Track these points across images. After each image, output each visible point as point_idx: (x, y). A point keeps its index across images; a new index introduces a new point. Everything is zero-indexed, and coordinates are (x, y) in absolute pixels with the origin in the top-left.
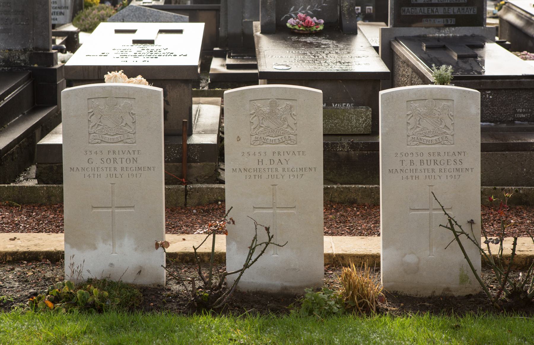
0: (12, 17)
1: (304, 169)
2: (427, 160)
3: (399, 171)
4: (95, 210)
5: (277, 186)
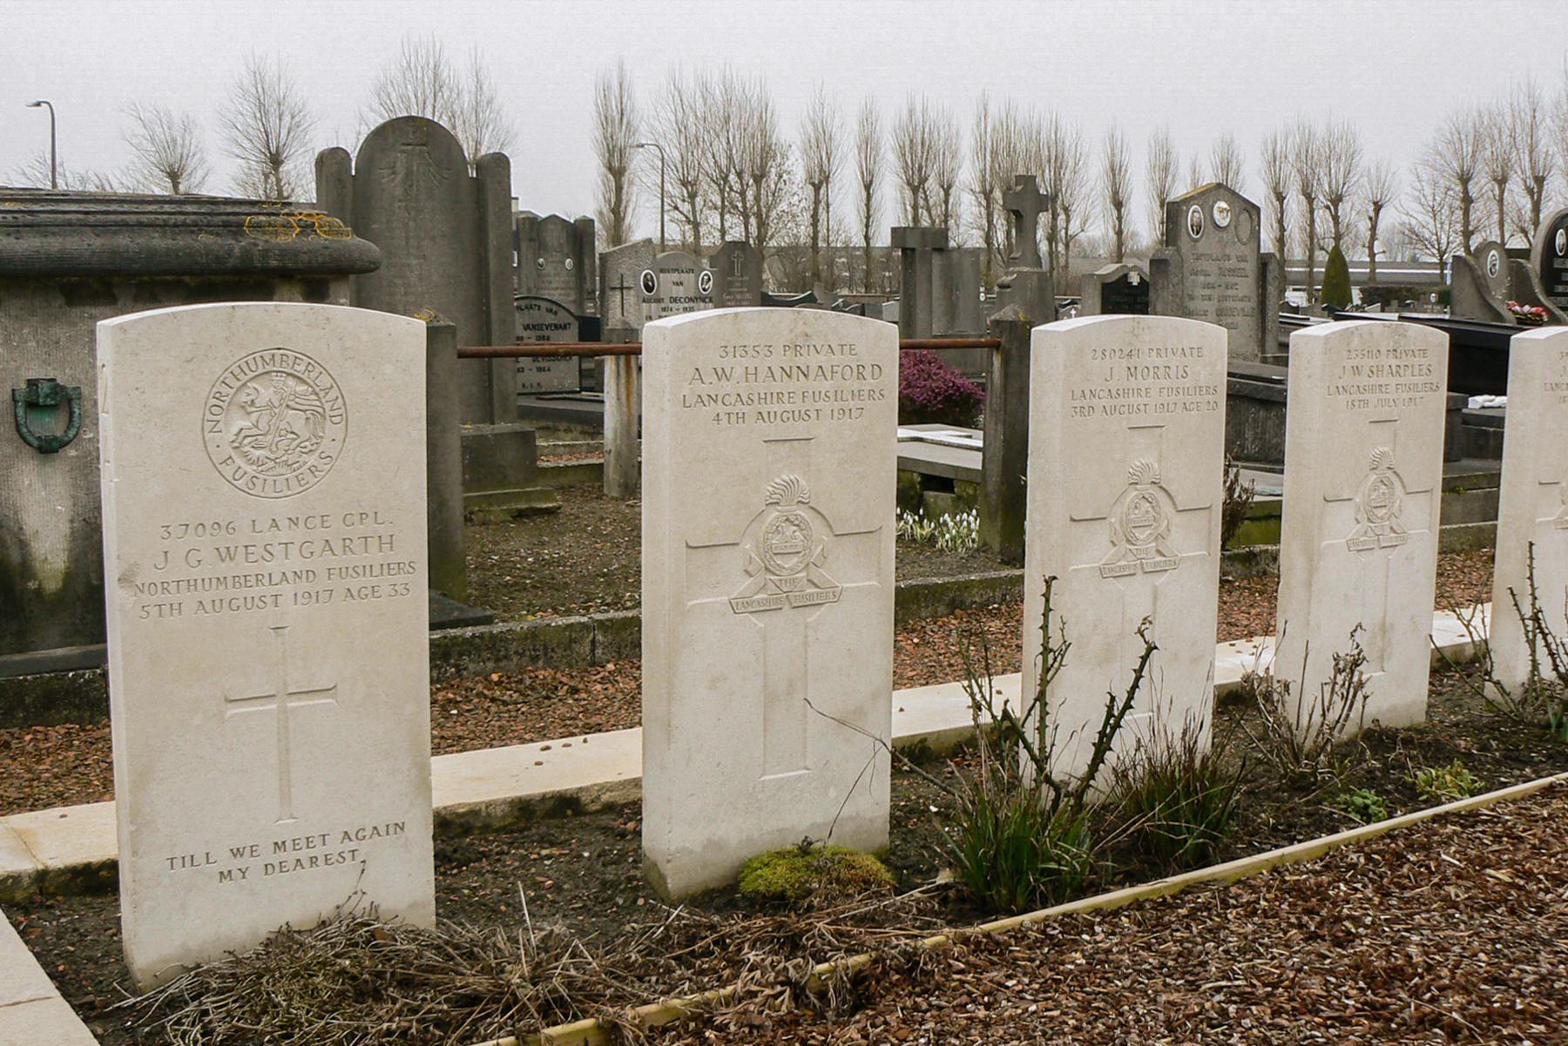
1: (230, 581)
2: (183, 858)
3: (290, 576)
5: (286, 631)
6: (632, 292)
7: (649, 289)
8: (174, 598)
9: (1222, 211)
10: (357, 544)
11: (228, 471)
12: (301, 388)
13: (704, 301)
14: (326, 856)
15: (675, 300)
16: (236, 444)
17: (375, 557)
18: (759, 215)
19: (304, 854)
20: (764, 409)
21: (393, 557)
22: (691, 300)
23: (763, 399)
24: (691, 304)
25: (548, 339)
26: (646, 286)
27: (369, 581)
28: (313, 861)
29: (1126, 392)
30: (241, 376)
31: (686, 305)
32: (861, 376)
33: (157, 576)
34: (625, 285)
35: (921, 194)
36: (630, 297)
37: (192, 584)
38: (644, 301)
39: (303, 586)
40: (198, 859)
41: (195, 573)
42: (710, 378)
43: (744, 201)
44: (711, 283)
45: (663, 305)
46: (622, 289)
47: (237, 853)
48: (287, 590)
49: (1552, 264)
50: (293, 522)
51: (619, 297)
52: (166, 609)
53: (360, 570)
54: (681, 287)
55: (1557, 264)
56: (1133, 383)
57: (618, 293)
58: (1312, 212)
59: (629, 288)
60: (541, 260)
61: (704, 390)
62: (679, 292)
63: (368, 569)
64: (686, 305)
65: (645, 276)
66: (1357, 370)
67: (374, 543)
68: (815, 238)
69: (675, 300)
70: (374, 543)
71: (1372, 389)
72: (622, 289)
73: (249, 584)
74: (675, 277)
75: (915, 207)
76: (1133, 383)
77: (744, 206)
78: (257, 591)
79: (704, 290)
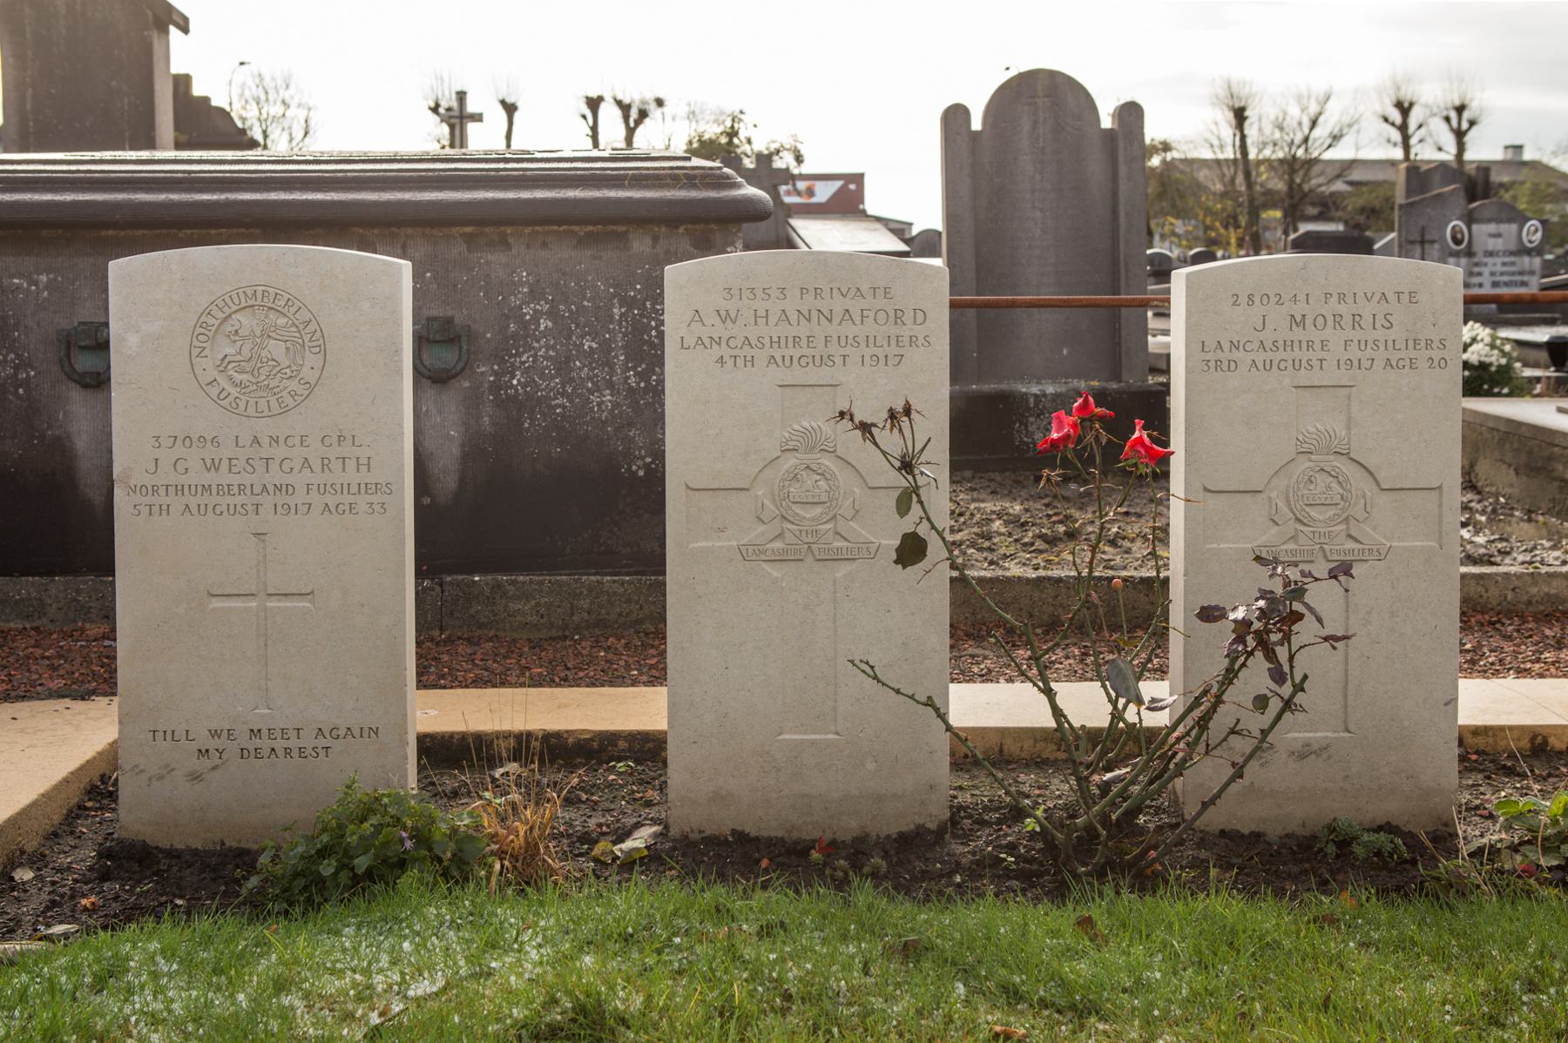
4: (217, 603)
6: (1436, 246)
7: (1457, 242)
10: (336, 466)
11: (214, 392)
15: (1491, 254)
16: (221, 368)
17: (352, 476)
19: (279, 744)
21: (370, 479)
22: (1512, 253)
23: (775, 343)
24: (1512, 259)
28: (287, 751)
30: (226, 309)
31: (1506, 260)
33: (148, 480)
34: (1427, 237)
37: (180, 490)
39: (281, 499)
40: (181, 734)
44: (1539, 235)
45: (1476, 260)
46: (1422, 242)
47: (215, 734)
48: (267, 501)
52: (156, 509)
53: (338, 488)
54: (1500, 241)
56: (1298, 334)
59: (1432, 242)
61: (704, 333)
62: (1498, 244)
63: (345, 486)
64: (1506, 260)
65: (1453, 227)
67: (351, 465)
69: (1491, 254)
70: (351, 465)
72: (1422, 242)
73: (232, 492)
74: (1492, 228)
78: (239, 500)
79: (1530, 242)
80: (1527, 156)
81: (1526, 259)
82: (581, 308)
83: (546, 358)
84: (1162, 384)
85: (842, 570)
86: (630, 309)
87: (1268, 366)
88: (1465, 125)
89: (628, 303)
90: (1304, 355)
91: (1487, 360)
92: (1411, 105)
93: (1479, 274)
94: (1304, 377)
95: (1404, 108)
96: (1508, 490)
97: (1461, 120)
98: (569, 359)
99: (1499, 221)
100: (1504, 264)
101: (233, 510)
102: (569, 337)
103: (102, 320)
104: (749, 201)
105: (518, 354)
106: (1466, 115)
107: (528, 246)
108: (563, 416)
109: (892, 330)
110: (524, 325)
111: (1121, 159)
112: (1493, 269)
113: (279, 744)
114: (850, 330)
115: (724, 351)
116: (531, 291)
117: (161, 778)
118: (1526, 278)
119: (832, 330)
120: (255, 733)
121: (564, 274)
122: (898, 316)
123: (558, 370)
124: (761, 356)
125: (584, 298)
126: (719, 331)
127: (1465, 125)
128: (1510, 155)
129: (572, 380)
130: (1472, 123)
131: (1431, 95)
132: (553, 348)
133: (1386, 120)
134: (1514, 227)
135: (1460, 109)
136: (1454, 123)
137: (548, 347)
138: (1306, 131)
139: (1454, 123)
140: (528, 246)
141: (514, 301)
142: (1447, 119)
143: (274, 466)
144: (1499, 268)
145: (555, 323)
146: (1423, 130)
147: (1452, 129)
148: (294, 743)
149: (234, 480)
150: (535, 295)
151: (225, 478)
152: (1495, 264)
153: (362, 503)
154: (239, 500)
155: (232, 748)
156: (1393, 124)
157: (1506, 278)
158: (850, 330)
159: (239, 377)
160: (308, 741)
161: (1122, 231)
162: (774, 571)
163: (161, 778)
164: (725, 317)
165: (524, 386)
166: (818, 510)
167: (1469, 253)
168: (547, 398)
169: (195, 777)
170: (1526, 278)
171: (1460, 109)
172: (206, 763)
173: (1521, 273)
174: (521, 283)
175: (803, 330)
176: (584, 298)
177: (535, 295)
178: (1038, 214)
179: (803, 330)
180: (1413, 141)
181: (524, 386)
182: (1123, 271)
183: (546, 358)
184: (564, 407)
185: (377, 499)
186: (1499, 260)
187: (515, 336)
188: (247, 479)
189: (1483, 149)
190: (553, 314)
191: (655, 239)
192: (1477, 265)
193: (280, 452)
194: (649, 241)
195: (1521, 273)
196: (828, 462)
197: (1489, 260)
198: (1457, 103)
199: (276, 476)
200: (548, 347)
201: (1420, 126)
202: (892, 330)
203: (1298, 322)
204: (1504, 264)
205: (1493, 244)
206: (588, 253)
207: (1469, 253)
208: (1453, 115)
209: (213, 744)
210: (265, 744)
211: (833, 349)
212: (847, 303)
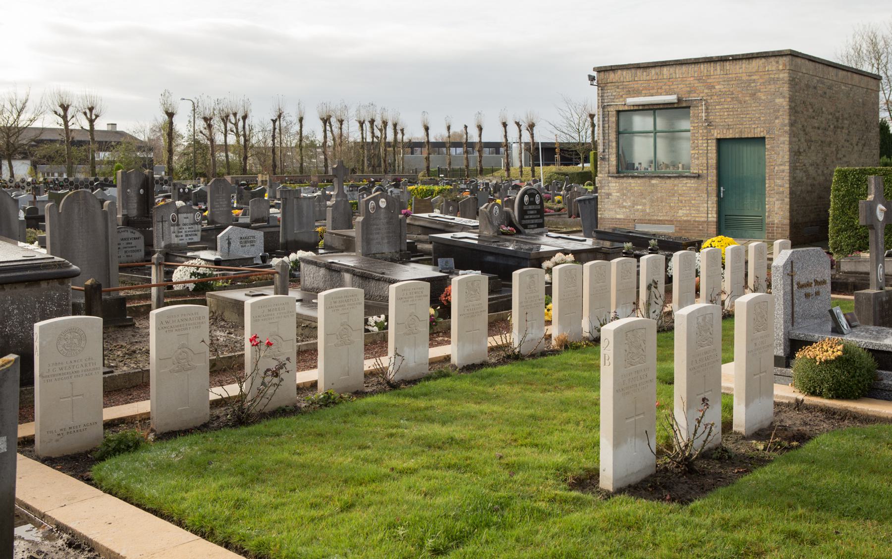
0: (391, 235)
4: (62, 400)
8: (50, 378)
9: (382, 202)
10: (88, 365)
11: (62, 352)
12: (77, 334)
13: (197, 224)
14: (288, 303)
15: (185, 225)
17: (92, 367)
18: (245, 135)
19: (75, 430)
20: (177, 329)
21: (96, 367)
22: (192, 224)
23: (177, 326)
25: (131, 243)
26: (173, 220)
27: (91, 372)
28: (77, 431)
29: (268, 315)
32: (200, 319)
33: (47, 374)
34: (164, 219)
35: (328, 124)
36: (166, 225)
37: (54, 375)
38: (172, 226)
40: (54, 431)
41: (55, 373)
42: (164, 323)
43: (237, 129)
46: (162, 222)
47: (61, 430)
48: (73, 375)
49: (523, 208)
50: (75, 361)
51: (161, 225)
54: (188, 220)
55: (525, 208)
56: (270, 313)
57: (161, 223)
58: (520, 131)
59: (166, 221)
60: (128, 190)
61: (163, 326)
62: (187, 221)
66: (335, 302)
67: (91, 365)
68: (274, 144)
69: (185, 225)
70: (91, 365)
71: (340, 306)
72: (162, 222)
74: (185, 215)
75: (325, 131)
76: (270, 313)
77: (237, 131)
78: (67, 376)
80: (118, 129)
81: (196, 226)
82: (27, 306)
83: (16, 322)
84: (313, 343)
85: (189, 372)
86: (41, 304)
87: (265, 320)
88: (94, 117)
89: (41, 303)
90: (270, 317)
91: (205, 272)
92: (68, 106)
93: (181, 232)
94: (271, 321)
95: (65, 108)
96: (236, 321)
97: (91, 113)
98: (23, 321)
99: (187, 213)
100: (189, 228)
101: (65, 378)
102: (23, 315)
103: (509, 294)
104: (74, 271)
105: (8, 322)
106: (94, 112)
107: (11, 289)
108: (21, 338)
109: (198, 321)
110: (10, 313)
111: (109, 221)
112: (186, 230)
113: (75, 430)
114: (191, 322)
115: (167, 329)
116: (12, 302)
117: (49, 442)
118: (196, 233)
119: (187, 322)
120: (70, 428)
121: (22, 296)
122: (199, 318)
123: (20, 325)
124: (174, 329)
125: (27, 302)
126: (166, 325)
127: (94, 117)
128: (110, 128)
129: (24, 327)
130: (97, 116)
131: (77, 104)
132: (18, 318)
133: (56, 113)
134: (192, 214)
135: (91, 109)
136: (89, 116)
137: (17, 318)
138: (15, 117)
139: (89, 116)
140: (11, 289)
141: (6, 306)
142: (85, 114)
143: (75, 367)
144: (188, 230)
145: (19, 311)
146: (74, 119)
147: (87, 118)
148: (79, 429)
149: (66, 371)
150: (13, 303)
151: (64, 371)
152: (186, 228)
153: (94, 372)
154: (67, 376)
155: (65, 433)
156: (60, 115)
157: (190, 233)
158: (191, 322)
159: (67, 348)
160: (82, 428)
161: (110, 245)
162: (176, 374)
163: (49, 442)
164: (167, 322)
165: (10, 331)
166: (185, 360)
167: (178, 225)
168: (17, 334)
169: (57, 441)
170: (196, 233)
171: (91, 109)
172: (59, 437)
173: (195, 231)
174: (8, 300)
175: (182, 323)
176: (27, 302)
177: (13, 303)
178: (81, 240)
179: (182, 323)
180: (70, 124)
181: (10, 331)
182: (110, 259)
183: (16, 322)
184: (22, 336)
185: (97, 371)
186: (187, 227)
187: (7, 316)
188: (69, 371)
189: (101, 125)
190: (18, 308)
191: (48, 283)
192: (180, 229)
193: (76, 364)
194: (46, 284)
195: (195, 231)
196: (187, 350)
197: (184, 227)
198: (90, 106)
199: (76, 369)
200: (17, 318)
201: (73, 117)
202: (198, 321)
203: (269, 310)
204: (189, 228)
205: (186, 221)
206: (28, 289)
207: (178, 225)
208: (88, 111)
209: (61, 432)
210: (72, 430)
211: (188, 327)
212: (190, 317)
